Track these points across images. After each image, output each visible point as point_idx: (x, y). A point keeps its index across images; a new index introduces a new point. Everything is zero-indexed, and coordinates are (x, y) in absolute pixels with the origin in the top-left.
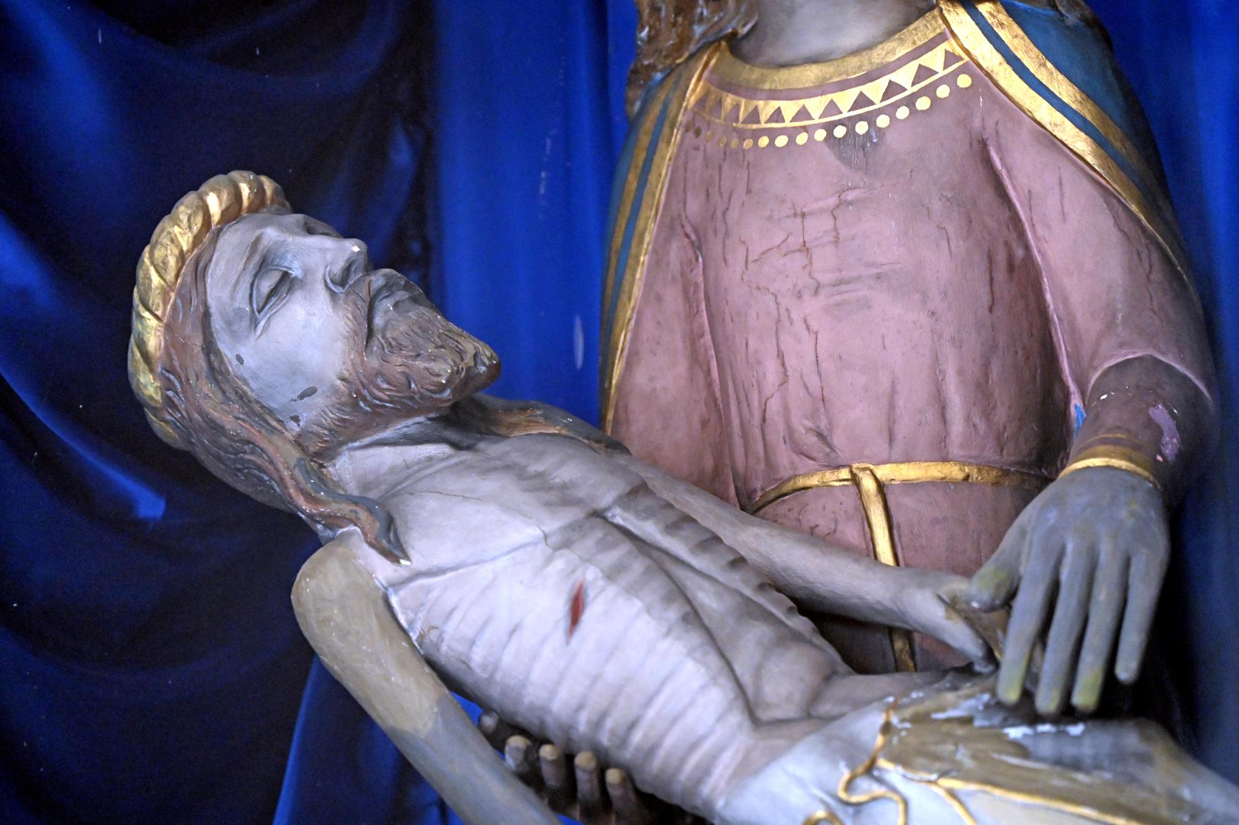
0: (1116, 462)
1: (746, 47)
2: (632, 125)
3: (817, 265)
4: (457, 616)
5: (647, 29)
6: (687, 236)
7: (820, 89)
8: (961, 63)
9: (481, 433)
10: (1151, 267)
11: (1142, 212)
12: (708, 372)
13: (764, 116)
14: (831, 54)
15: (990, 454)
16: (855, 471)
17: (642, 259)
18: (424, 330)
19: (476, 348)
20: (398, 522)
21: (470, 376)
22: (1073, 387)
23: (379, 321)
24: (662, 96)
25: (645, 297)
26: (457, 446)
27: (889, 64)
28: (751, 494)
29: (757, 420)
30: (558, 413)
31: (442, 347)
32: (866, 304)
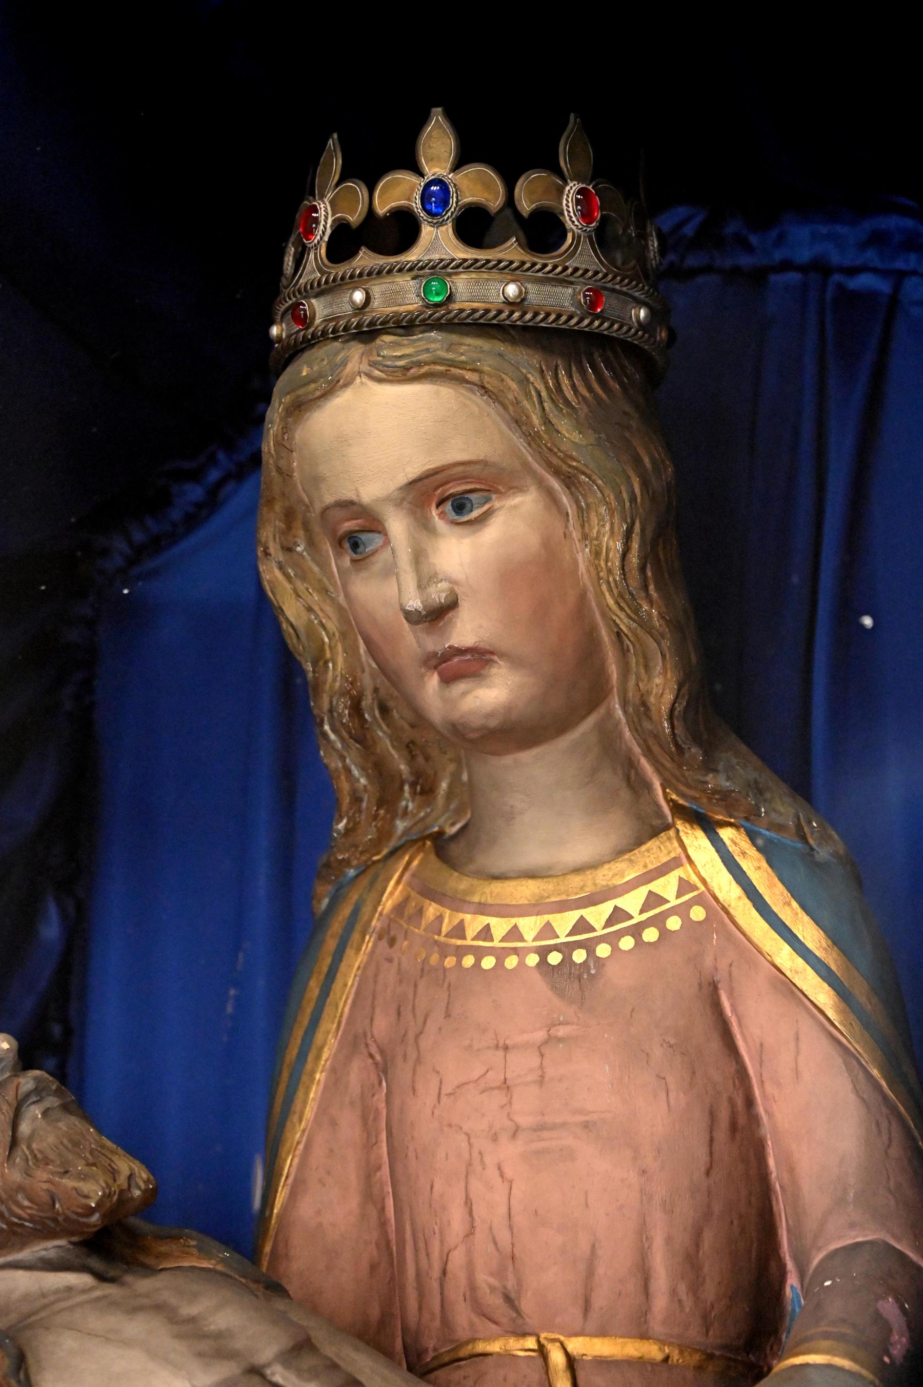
0: (839, 1361)
1: (455, 850)
2: (319, 924)
3: (516, 1106)
5: (345, 821)
6: (371, 1056)
7: (535, 908)
8: (696, 893)
9: (127, 1263)
10: (890, 1140)
11: (885, 1077)
12: (383, 1209)
13: (470, 932)
14: (550, 868)
15: (694, 1333)
16: (543, 1341)
17: (318, 1076)
18: (76, 1144)
19: (131, 1169)
20: (30, 1361)
21: (123, 1198)
22: (790, 1265)
23: (25, 1128)
24: (354, 896)
25: (317, 1120)
26: (101, 1277)
27: (615, 887)
28: (421, 1353)
29: (436, 1273)
30: (213, 1245)
31: (94, 1165)
32: (568, 1155)
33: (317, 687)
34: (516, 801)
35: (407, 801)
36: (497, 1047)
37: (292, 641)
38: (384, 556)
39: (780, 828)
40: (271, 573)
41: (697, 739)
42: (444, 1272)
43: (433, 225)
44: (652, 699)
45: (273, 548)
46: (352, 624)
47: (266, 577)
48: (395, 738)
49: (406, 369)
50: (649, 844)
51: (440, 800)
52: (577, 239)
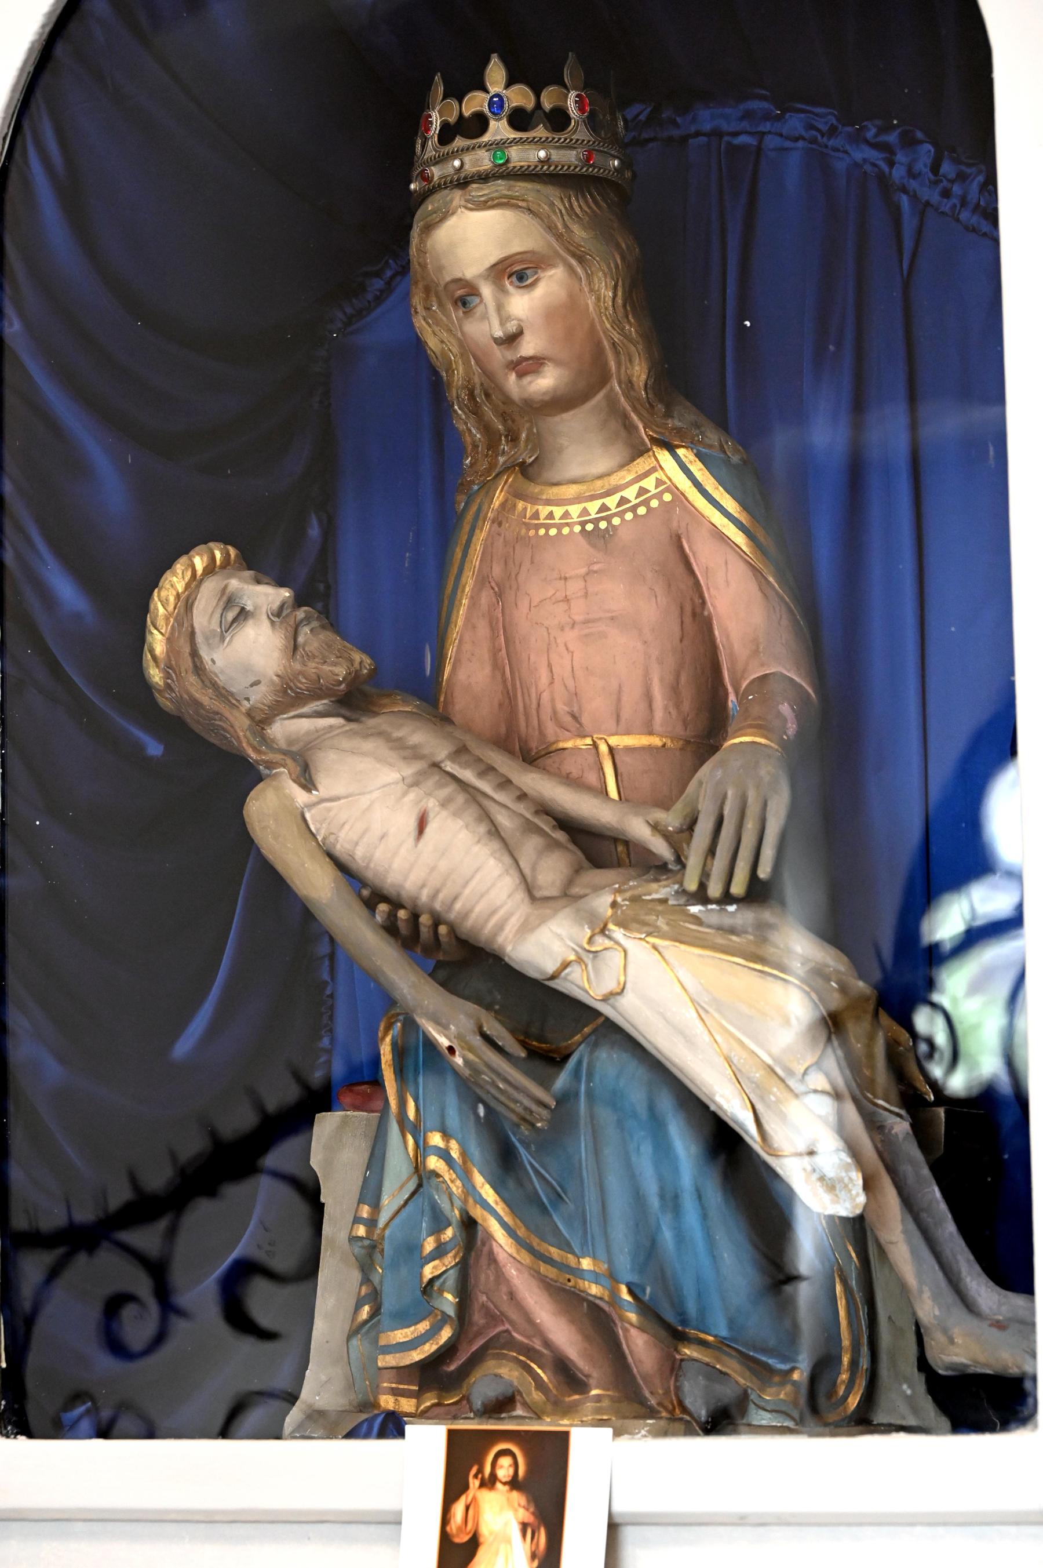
1: (531, 470)
4: (347, 827)
6: (493, 588)
13: (542, 515)
15: (679, 730)
18: (329, 646)
20: (311, 767)
22: (730, 689)
23: (301, 639)
25: (465, 625)
26: (348, 719)
28: (530, 750)
29: (534, 706)
33: (449, 384)
34: (564, 441)
35: (504, 446)
36: (560, 579)
37: (434, 360)
38: (480, 309)
39: (711, 446)
40: (419, 322)
41: (661, 401)
42: (539, 705)
43: (496, 120)
44: (635, 379)
45: (420, 308)
46: (466, 349)
47: (417, 325)
48: (495, 408)
49: (486, 202)
50: (638, 461)
51: (522, 444)
52: (577, 123)
